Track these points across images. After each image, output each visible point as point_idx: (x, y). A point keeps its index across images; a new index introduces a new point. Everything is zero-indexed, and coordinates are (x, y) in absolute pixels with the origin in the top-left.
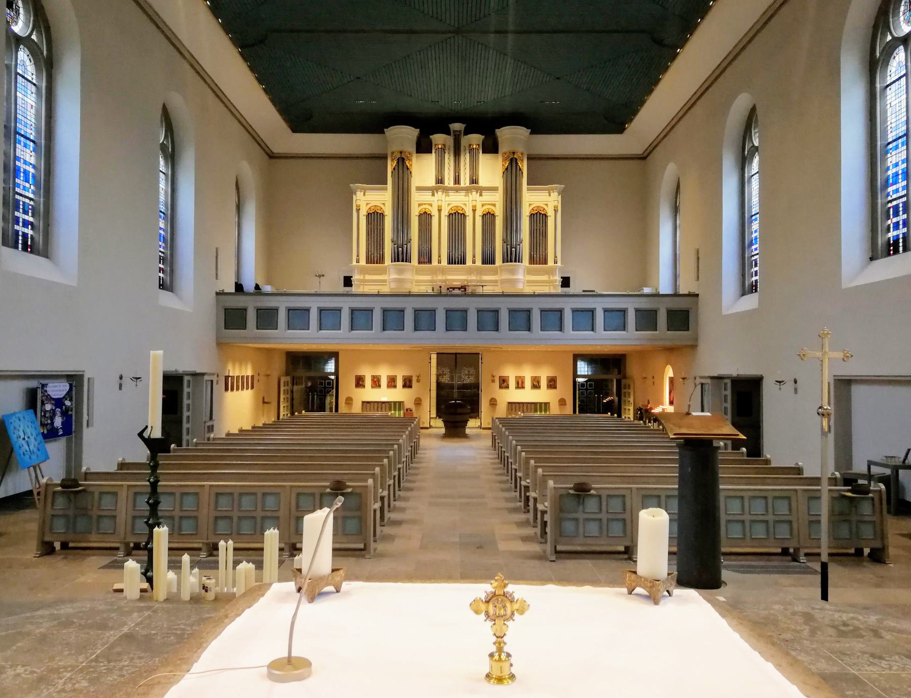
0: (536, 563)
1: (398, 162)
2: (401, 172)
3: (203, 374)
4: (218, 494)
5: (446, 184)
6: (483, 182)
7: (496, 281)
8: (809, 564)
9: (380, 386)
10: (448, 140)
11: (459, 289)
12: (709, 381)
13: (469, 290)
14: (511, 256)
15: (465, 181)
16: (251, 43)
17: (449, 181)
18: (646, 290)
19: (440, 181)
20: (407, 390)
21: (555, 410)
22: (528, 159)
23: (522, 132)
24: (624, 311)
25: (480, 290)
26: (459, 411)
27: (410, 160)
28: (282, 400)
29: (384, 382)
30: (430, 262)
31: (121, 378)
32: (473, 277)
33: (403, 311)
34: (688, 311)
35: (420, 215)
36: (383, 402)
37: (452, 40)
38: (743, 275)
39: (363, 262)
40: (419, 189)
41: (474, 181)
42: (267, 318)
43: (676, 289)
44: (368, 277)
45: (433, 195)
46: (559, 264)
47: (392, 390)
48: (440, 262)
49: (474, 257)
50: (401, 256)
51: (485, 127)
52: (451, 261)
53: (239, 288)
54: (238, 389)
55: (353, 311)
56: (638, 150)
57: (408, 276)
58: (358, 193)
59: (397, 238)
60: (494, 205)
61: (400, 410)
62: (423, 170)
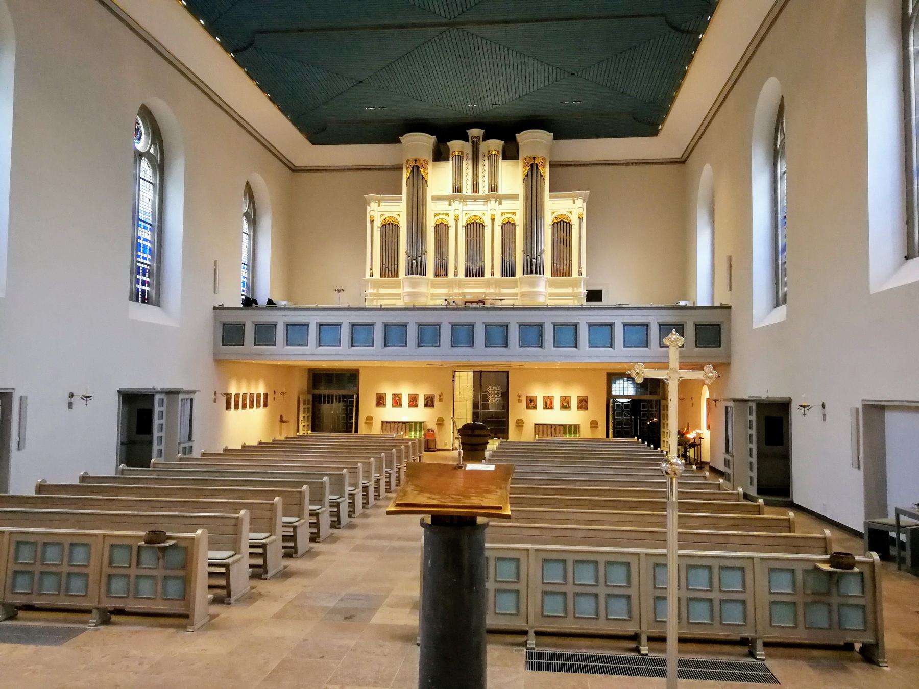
0: (399, 645)
1: (413, 171)
2: (415, 179)
3: (177, 392)
4: (19, 543)
5: (464, 193)
6: (503, 190)
7: (516, 295)
8: (767, 663)
9: (401, 405)
10: (467, 147)
11: (477, 303)
12: (731, 404)
13: (488, 304)
14: (533, 268)
15: (484, 189)
16: (242, 49)
17: (467, 190)
18: (682, 303)
19: (457, 189)
20: (429, 410)
21: (585, 433)
22: (551, 166)
23: (542, 137)
24: (646, 326)
25: (498, 304)
26: (477, 432)
27: (426, 168)
28: (301, 418)
29: (405, 401)
30: (446, 274)
31: (71, 396)
32: (491, 291)
33: (406, 326)
34: (719, 325)
35: (437, 226)
36: (404, 422)
37: (447, 32)
38: (777, 284)
39: (377, 275)
40: (435, 198)
41: (493, 189)
42: (265, 334)
43: (713, 302)
44: (382, 291)
45: (450, 204)
46: (584, 275)
47: (414, 409)
48: (456, 275)
49: (492, 268)
50: (417, 268)
51: (505, 132)
52: (468, 274)
53: (249, 302)
54: (244, 407)
55: (353, 325)
56: (677, 154)
57: (423, 289)
58: (372, 204)
59: (409, 250)
60: (515, 214)
61: (420, 430)
62: (439, 178)
